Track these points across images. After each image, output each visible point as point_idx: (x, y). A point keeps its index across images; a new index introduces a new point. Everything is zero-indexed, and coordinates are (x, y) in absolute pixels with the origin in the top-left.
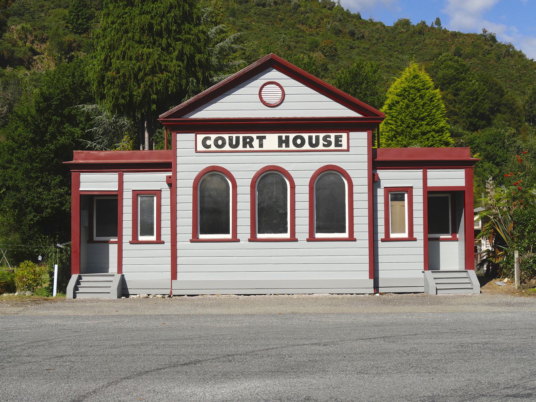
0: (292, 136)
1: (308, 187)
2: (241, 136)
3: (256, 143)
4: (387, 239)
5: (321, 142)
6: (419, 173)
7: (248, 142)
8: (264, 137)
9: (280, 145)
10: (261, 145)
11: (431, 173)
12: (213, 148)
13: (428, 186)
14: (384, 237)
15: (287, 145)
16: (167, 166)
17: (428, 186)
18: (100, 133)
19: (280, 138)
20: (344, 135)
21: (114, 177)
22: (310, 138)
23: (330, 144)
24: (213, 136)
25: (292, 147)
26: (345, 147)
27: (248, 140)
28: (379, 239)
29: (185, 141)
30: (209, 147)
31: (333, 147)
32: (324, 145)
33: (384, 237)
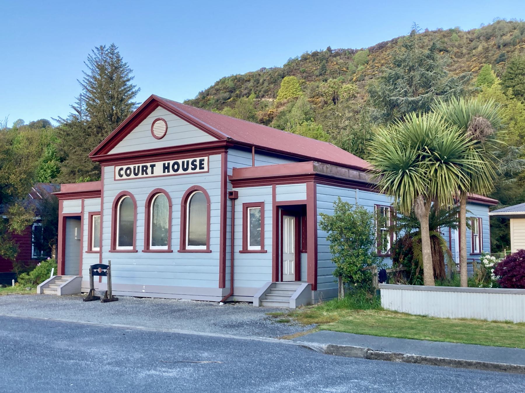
0: (172, 162)
1: (265, 216)
2: (141, 165)
3: (149, 170)
4: (245, 251)
5: (190, 166)
6: (268, 189)
7: (145, 171)
8: (154, 165)
9: (164, 172)
10: (152, 173)
12: (125, 177)
13: (306, 199)
14: (242, 250)
15: (168, 172)
16: (97, 193)
17: (306, 199)
18: (317, 73)
19: (164, 164)
20: (206, 158)
21: (79, 202)
22: (183, 162)
23: (196, 166)
24: (125, 167)
25: (172, 172)
27: (145, 168)
30: (121, 176)
31: (198, 170)
32: (192, 169)
33: (242, 250)
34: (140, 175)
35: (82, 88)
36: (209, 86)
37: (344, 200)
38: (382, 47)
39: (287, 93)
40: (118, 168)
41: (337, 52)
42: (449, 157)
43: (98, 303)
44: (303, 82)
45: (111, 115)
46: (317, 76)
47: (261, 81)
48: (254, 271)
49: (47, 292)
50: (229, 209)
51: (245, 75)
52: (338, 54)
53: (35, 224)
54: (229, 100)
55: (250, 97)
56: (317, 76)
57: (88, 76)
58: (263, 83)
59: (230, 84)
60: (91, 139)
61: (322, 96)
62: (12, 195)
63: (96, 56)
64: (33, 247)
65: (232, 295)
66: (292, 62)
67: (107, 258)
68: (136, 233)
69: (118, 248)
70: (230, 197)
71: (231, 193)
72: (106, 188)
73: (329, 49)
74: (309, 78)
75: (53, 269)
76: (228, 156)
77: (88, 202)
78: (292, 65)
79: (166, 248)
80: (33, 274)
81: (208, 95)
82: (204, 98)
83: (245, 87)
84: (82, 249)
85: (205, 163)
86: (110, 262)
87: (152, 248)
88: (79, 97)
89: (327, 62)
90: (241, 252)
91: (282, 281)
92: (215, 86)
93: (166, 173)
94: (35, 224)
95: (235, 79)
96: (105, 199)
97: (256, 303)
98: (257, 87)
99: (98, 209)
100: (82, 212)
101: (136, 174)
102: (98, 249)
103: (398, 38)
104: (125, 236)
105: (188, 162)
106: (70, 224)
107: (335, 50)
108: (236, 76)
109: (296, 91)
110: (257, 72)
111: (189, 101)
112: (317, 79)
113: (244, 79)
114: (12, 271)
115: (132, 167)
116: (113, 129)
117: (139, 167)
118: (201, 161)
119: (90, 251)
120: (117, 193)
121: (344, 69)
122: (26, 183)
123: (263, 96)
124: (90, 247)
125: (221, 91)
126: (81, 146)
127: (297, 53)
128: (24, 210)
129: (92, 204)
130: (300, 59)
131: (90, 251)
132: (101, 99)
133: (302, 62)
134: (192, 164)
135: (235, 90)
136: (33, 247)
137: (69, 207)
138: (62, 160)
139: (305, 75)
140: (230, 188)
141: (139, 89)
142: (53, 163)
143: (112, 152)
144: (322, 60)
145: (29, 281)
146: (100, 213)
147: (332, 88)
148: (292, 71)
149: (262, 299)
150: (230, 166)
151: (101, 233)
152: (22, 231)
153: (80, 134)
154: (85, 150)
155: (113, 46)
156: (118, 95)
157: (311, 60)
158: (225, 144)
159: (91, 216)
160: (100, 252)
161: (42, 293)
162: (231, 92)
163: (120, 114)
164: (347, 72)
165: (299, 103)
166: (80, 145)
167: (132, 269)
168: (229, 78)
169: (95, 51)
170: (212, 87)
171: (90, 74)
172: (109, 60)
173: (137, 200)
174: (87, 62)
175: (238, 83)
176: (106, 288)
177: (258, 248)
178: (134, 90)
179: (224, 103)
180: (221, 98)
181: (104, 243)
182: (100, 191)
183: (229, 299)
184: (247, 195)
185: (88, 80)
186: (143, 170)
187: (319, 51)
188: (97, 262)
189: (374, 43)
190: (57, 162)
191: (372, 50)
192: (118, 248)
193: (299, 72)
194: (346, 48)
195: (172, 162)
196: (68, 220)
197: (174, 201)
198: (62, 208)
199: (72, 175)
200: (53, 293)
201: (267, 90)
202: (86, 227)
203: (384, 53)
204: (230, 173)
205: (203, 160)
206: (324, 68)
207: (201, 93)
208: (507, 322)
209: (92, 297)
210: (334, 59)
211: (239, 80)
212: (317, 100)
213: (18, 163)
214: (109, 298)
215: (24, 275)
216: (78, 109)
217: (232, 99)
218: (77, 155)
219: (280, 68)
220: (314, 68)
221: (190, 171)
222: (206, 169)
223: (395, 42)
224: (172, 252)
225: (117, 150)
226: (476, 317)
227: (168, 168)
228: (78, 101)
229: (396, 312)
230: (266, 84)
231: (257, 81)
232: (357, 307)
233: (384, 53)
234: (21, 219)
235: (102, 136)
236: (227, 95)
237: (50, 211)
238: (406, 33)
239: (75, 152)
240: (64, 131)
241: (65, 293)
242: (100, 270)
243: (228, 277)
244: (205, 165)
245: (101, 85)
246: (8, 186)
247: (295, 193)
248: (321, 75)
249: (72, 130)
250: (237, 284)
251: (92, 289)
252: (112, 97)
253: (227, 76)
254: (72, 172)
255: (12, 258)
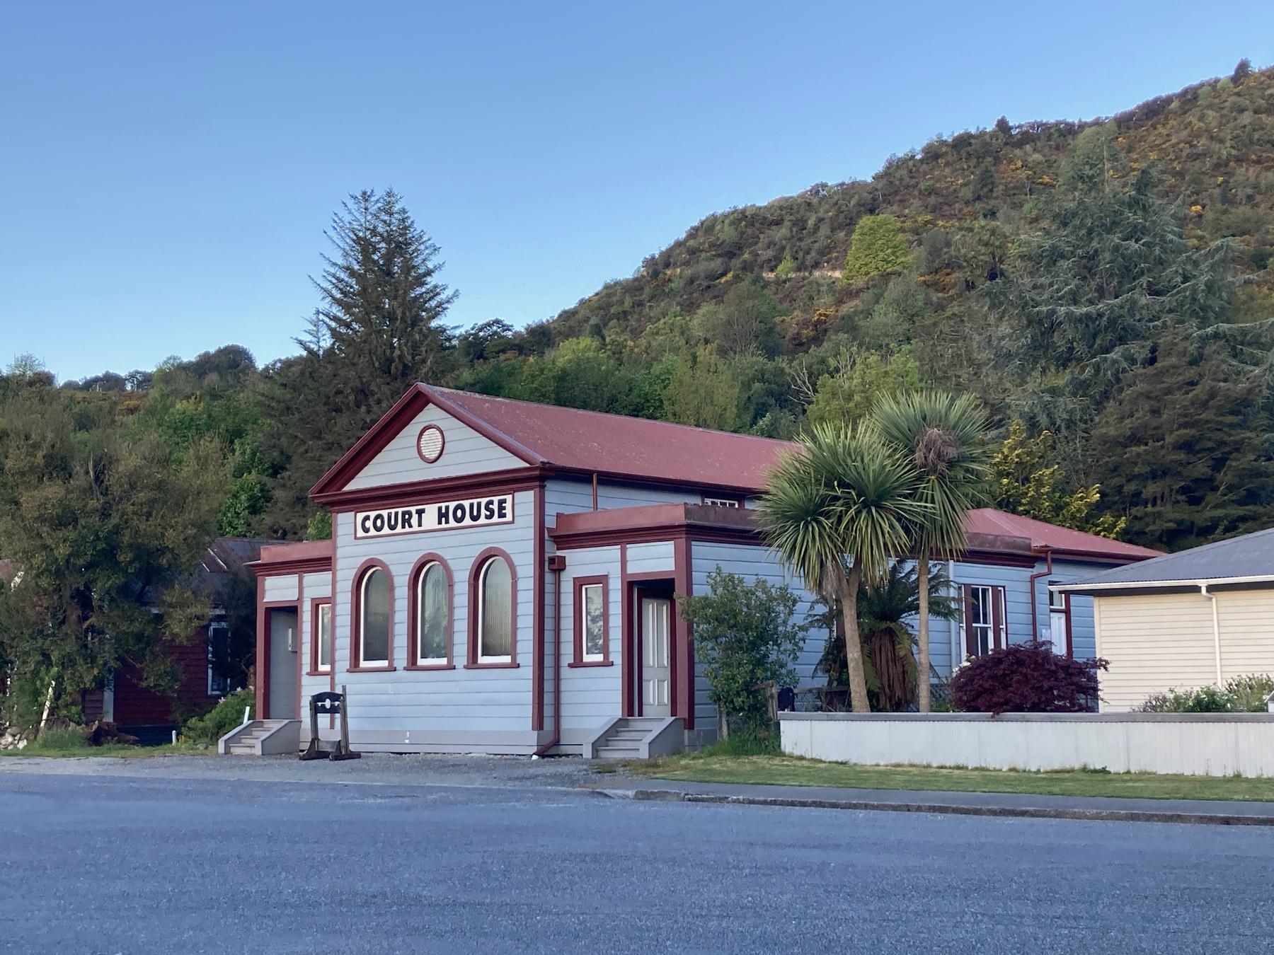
0: (452, 505)
2: (400, 510)
4: (578, 663)
5: (483, 511)
6: (613, 552)
7: (406, 521)
8: (423, 511)
9: (440, 523)
10: (420, 525)
11: (634, 550)
12: (373, 532)
15: (447, 522)
16: (325, 563)
18: (967, 193)
19: (440, 509)
20: (509, 498)
21: (293, 579)
22: (472, 506)
23: (492, 512)
24: (373, 514)
25: (452, 523)
26: (509, 518)
28: (304, 672)
29: (346, 522)
30: (366, 530)
31: (495, 519)
32: (487, 517)
34: (399, 529)
35: (321, 295)
36: (672, 242)
37: (727, 569)
38: (1154, 111)
39: (868, 260)
40: (361, 516)
41: (1027, 132)
42: (874, 498)
43: (327, 761)
44: (927, 222)
45: (390, 361)
46: (967, 203)
47: (811, 222)
48: (593, 698)
49: (236, 750)
50: (549, 588)
51: (769, 208)
52: (1029, 137)
53: (214, 625)
54: (723, 280)
55: (780, 268)
56: (967, 203)
57: (335, 264)
58: (816, 228)
59: (727, 234)
60: (343, 420)
61: (960, 267)
62: (168, 569)
63: (355, 217)
64: (210, 671)
65: (557, 743)
66: (898, 167)
67: (344, 678)
68: (393, 636)
69: (364, 664)
70: (549, 567)
71: (552, 560)
72: (340, 553)
73: (1003, 125)
74: (946, 207)
75: (248, 708)
76: (547, 493)
77: (309, 578)
78: (898, 175)
79: (444, 661)
80: (210, 719)
81: (667, 265)
82: (655, 274)
83: (766, 240)
84: (301, 670)
85: (508, 505)
86: (344, 688)
87: (421, 662)
88: (314, 318)
89: (997, 161)
90: (570, 666)
91: (640, 714)
92: (686, 240)
93: (444, 525)
94: (214, 625)
95: (740, 220)
96: (340, 575)
97: (587, 754)
98: (800, 240)
99: (326, 592)
100: (300, 599)
101: (392, 528)
102: (327, 668)
103: (1202, 85)
104: (372, 643)
105: (479, 505)
106: (278, 622)
107: (1020, 126)
108: (743, 212)
109: (893, 254)
110: (802, 196)
111: (616, 283)
112: (966, 210)
113: (765, 218)
114: (170, 718)
115: (385, 513)
116: (395, 394)
117: (396, 514)
118: (501, 502)
119: (314, 671)
120: (359, 562)
121: (1046, 179)
122: (196, 546)
123: (816, 265)
124: (320, 663)
125: (703, 255)
126: (319, 438)
127: (912, 143)
128: (192, 597)
129: (316, 584)
130: (918, 157)
131: (314, 671)
132: (364, 321)
133: (925, 167)
134: (487, 508)
135: (740, 249)
136: (210, 671)
137: (277, 590)
138: (276, 470)
139: (932, 200)
140: (551, 550)
141: (456, 294)
142: (252, 477)
143: (350, 487)
144: (981, 157)
145: (203, 733)
146: (330, 600)
147: (986, 245)
148: (896, 193)
149: (596, 747)
150: (551, 510)
151: (333, 638)
152: (189, 639)
153: (317, 408)
154: (329, 447)
155: (389, 194)
156: (404, 313)
157: (949, 158)
158: (537, 473)
159: (316, 605)
160: (331, 674)
161: (227, 752)
162: (731, 255)
163: (409, 358)
164: (1053, 186)
165: (894, 289)
166: (317, 435)
167: (392, 705)
168: (726, 216)
169: (350, 203)
170: (679, 244)
171: (340, 261)
172: (381, 228)
173: (394, 573)
174: (332, 233)
175: (750, 231)
176: (337, 737)
177: (599, 658)
178: (443, 296)
179: (709, 287)
180: (702, 275)
181: (338, 655)
182: (330, 558)
183: (550, 750)
184: (581, 561)
185: (334, 276)
186: (404, 521)
187: (973, 131)
188: (328, 689)
189: (1130, 102)
190: (265, 479)
191: (1125, 122)
192: (364, 664)
193: (916, 193)
194: (1052, 121)
195: (452, 505)
196: (273, 614)
197: (520, 572)
198: (264, 591)
199: (299, 507)
200: (248, 751)
201: (828, 247)
202: (307, 627)
203: (1161, 129)
204: (550, 522)
205: (505, 501)
206: (987, 181)
207: (650, 263)
208: (958, 768)
209: (315, 753)
210: (1018, 152)
211: (751, 223)
212: (947, 279)
213: (180, 506)
214: (342, 753)
215: (193, 721)
216: (312, 346)
217: (730, 275)
218: (312, 459)
219: (866, 184)
220: (959, 181)
221: (482, 520)
222: (509, 518)
223: (1190, 97)
224: (454, 668)
225: (359, 483)
226: (916, 762)
227: (446, 515)
228: (312, 327)
229: (802, 758)
230: (824, 230)
231: (801, 224)
232: (739, 750)
233: (1161, 129)
234: (186, 613)
235: (369, 412)
236: (716, 264)
237: (242, 594)
238: (1225, 71)
239: (307, 451)
240: (279, 402)
241: (270, 749)
242: (329, 703)
243: (548, 711)
244: (508, 511)
245: (363, 293)
246: (162, 551)
247: (655, 558)
248: (979, 198)
249: (303, 373)
250: (565, 724)
251: (315, 739)
252: (391, 316)
253: (719, 212)
254: (299, 499)
255: (170, 693)
